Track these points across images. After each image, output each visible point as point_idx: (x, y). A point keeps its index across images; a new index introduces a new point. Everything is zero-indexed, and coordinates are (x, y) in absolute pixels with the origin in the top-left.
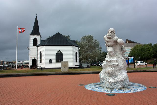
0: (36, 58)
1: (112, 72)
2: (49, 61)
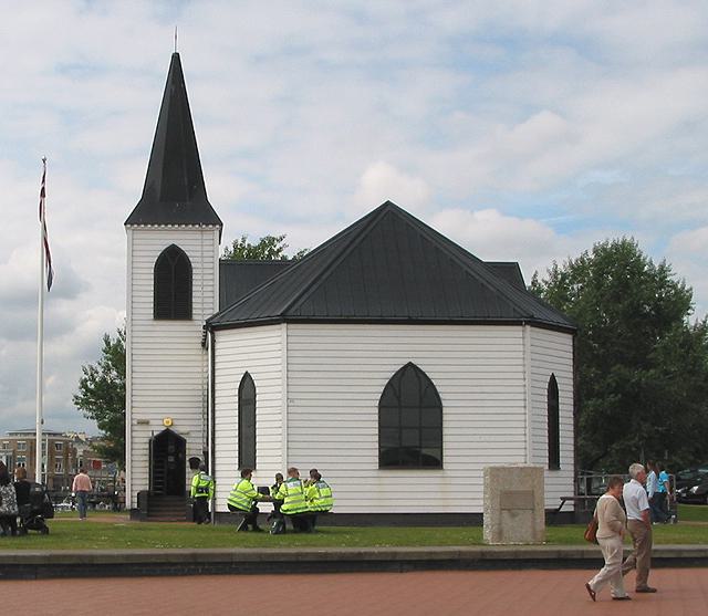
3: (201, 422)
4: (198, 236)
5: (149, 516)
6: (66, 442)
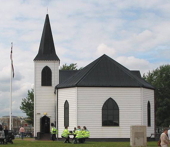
3: (54, 114)
4: (53, 63)
5: (40, 139)
6: (18, 119)
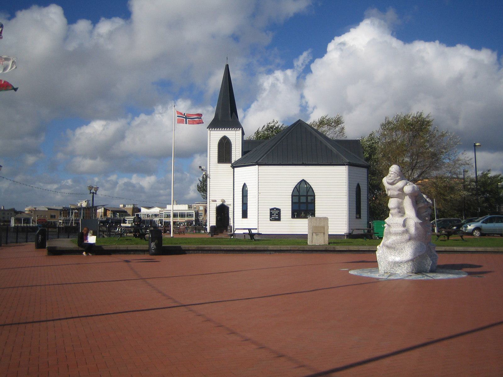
0: (228, 202)
1: (392, 244)
2: (271, 214)
4: (234, 132)
